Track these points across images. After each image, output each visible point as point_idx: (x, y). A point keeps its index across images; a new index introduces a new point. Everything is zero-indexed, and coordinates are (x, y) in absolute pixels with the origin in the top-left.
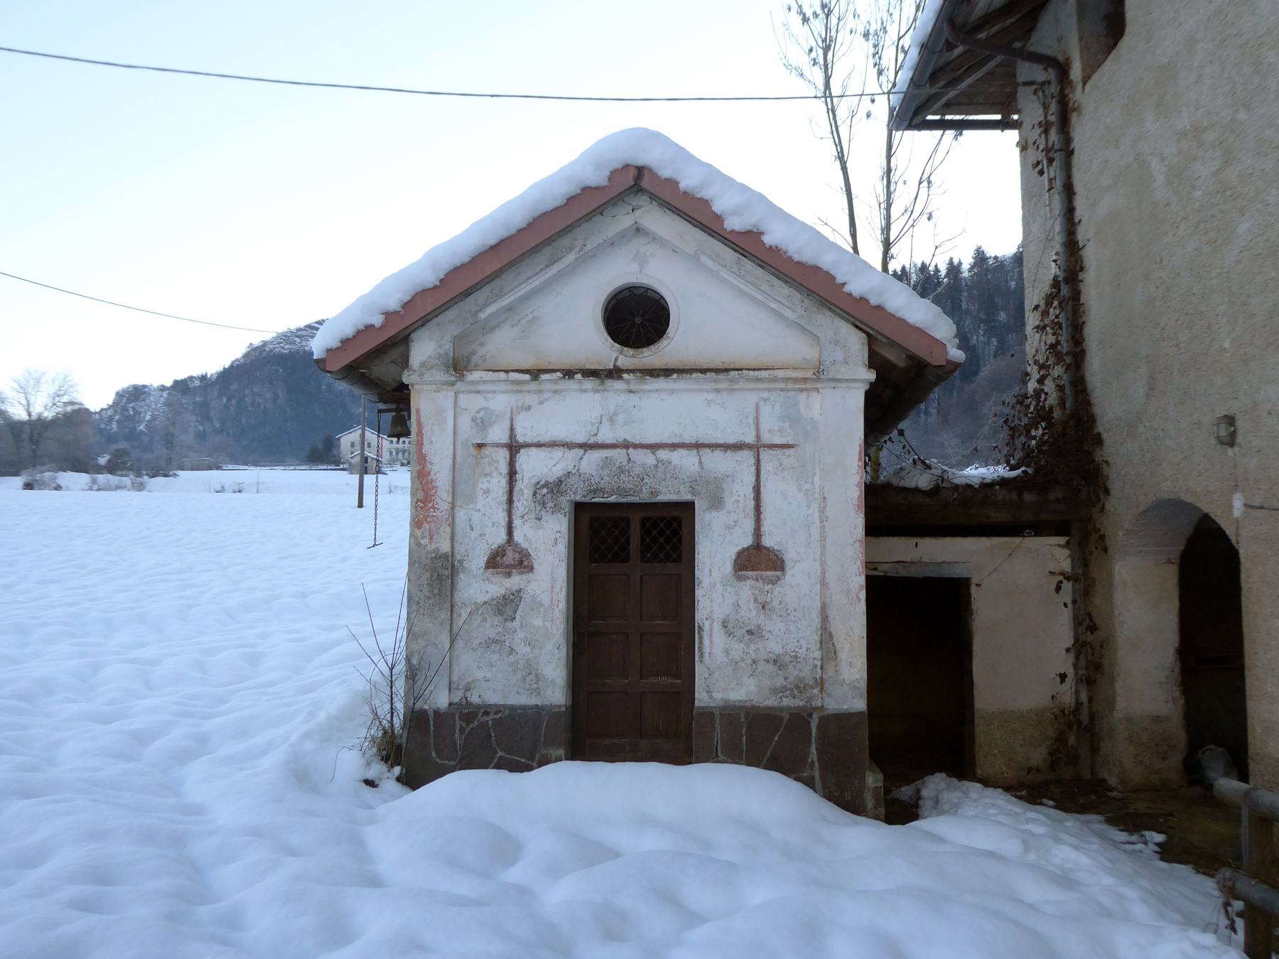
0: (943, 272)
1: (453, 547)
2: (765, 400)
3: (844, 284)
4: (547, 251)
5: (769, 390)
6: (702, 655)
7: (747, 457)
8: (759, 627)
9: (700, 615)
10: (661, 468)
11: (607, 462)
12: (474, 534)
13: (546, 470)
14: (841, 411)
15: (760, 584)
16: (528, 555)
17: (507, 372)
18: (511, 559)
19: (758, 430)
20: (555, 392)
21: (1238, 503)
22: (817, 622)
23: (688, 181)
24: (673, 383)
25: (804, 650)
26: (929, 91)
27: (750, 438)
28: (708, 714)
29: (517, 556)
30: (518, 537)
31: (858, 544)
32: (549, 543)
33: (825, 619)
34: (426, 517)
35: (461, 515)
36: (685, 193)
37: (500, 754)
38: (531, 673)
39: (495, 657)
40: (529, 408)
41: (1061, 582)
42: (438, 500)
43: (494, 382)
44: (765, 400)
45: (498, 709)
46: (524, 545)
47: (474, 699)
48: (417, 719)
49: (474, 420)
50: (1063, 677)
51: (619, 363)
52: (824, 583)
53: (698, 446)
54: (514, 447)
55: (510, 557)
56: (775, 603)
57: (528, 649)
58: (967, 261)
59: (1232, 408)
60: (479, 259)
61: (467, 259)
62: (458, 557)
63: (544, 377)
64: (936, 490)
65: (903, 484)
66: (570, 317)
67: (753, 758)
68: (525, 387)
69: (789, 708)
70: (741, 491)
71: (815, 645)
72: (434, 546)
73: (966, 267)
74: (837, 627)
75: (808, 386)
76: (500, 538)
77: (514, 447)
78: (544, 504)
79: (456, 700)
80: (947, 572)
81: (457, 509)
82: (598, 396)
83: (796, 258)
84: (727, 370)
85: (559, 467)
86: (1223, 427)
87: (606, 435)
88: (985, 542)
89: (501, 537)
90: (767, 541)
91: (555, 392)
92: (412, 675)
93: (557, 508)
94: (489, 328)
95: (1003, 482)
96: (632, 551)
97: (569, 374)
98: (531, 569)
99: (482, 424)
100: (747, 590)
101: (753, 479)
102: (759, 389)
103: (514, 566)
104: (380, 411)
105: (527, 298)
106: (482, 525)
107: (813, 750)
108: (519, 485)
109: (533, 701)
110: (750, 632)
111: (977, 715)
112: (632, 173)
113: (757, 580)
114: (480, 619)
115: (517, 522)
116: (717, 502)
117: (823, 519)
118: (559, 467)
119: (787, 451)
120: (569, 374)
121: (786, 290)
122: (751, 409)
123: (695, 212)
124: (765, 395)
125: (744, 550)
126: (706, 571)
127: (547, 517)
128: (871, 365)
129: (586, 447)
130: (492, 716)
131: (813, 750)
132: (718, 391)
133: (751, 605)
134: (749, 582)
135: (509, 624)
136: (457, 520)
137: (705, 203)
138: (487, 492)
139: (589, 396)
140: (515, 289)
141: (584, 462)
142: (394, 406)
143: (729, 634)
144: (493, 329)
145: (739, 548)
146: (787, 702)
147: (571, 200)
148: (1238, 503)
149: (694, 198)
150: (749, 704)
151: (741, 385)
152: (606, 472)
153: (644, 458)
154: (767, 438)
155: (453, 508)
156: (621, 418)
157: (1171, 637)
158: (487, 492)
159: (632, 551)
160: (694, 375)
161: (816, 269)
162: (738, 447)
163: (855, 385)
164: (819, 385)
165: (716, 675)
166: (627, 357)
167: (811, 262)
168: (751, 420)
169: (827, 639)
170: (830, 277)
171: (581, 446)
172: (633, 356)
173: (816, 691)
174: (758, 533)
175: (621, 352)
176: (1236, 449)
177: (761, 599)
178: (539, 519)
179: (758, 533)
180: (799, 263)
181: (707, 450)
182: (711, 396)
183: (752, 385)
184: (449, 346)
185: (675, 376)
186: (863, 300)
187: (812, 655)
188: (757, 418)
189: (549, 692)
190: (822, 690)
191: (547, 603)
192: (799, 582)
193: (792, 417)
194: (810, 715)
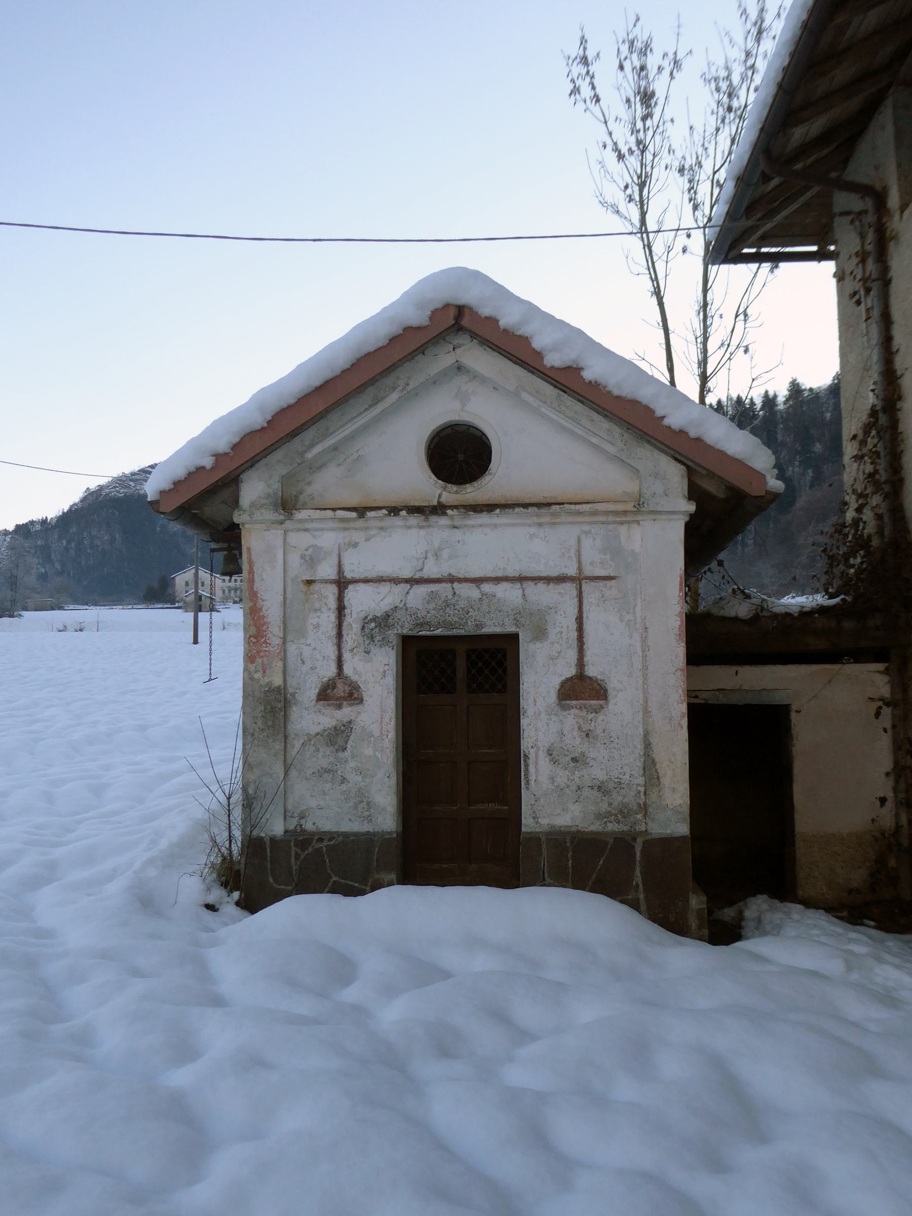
1: (285, 681)
3: (663, 417)
5: (591, 523)
6: (528, 782)
7: (569, 589)
8: (583, 754)
9: (526, 744)
10: (486, 601)
11: (433, 596)
12: (305, 668)
14: (662, 543)
17: (334, 510)
18: (339, 691)
19: (579, 562)
20: (381, 528)
22: (640, 748)
23: (508, 319)
25: (627, 776)
26: (744, 223)
27: (572, 571)
28: (534, 839)
29: (347, 689)
30: (348, 670)
31: (679, 673)
33: (647, 745)
34: (258, 652)
35: (292, 649)
37: (334, 879)
38: (362, 800)
39: (328, 786)
40: (355, 545)
42: (270, 635)
44: (587, 533)
45: (332, 835)
46: (354, 678)
47: (309, 826)
48: (254, 846)
49: (303, 557)
50: (883, 801)
51: (443, 500)
52: (646, 711)
53: (521, 579)
54: (342, 583)
55: (341, 689)
57: (360, 778)
58: (782, 393)
61: (293, 401)
62: (291, 690)
63: (370, 514)
64: (756, 619)
65: (722, 613)
66: (394, 455)
68: (353, 525)
69: (613, 832)
70: (565, 621)
71: (638, 771)
72: (267, 680)
73: (781, 399)
74: (659, 754)
75: (629, 518)
76: (330, 671)
77: (342, 583)
78: (372, 638)
79: (292, 827)
80: (767, 699)
82: (422, 532)
83: (616, 392)
84: (549, 505)
87: (432, 570)
89: (332, 671)
91: (381, 528)
92: (248, 804)
93: (385, 642)
94: (317, 466)
95: (822, 610)
96: (458, 683)
97: (394, 511)
98: (361, 701)
99: (311, 561)
100: (571, 719)
101: (576, 611)
102: (580, 523)
103: (344, 699)
104: (213, 550)
105: (352, 437)
107: (638, 873)
108: (348, 620)
109: (366, 828)
110: (574, 760)
112: (452, 313)
113: (581, 708)
114: (313, 748)
115: (346, 656)
116: (540, 634)
117: (645, 648)
120: (394, 511)
122: (573, 542)
124: (586, 528)
125: (568, 680)
126: (531, 701)
127: (375, 650)
131: (638, 873)
132: (540, 525)
133: (576, 734)
134: (573, 711)
137: (525, 341)
138: (317, 626)
139: (414, 532)
140: (342, 428)
142: (225, 545)
143: (555, 762)
145: (563, 678)
146: (611, 827)
147: (394, 340)
151: (563, 519)
152: (432, 605)
154: (588, 571)
155: (284, 643)
156: (445, 553)
159: (458, 683)
160: (517, 510)
161: (635, 403)
162: (561, 579)
166: (450, 494)
168: (573, 553)
169: (649, 766)
170: (648, 411)
171: (407, 581)
172: (456, 492)
174: (581, 663)
175: (445, 489)
178: (368, 653)
179: (581, 663)
180: (618, 398)
181: (530, 583)
182: (533, 530)
183: (571, 519)
184: (277, 486)
185: (498, 511)
186: (682, 433)
187: (635, 782)
188: (579, 552)
190: (645, 815)
191: (376, 733)
192: (622, 709)
194: (634, 839)
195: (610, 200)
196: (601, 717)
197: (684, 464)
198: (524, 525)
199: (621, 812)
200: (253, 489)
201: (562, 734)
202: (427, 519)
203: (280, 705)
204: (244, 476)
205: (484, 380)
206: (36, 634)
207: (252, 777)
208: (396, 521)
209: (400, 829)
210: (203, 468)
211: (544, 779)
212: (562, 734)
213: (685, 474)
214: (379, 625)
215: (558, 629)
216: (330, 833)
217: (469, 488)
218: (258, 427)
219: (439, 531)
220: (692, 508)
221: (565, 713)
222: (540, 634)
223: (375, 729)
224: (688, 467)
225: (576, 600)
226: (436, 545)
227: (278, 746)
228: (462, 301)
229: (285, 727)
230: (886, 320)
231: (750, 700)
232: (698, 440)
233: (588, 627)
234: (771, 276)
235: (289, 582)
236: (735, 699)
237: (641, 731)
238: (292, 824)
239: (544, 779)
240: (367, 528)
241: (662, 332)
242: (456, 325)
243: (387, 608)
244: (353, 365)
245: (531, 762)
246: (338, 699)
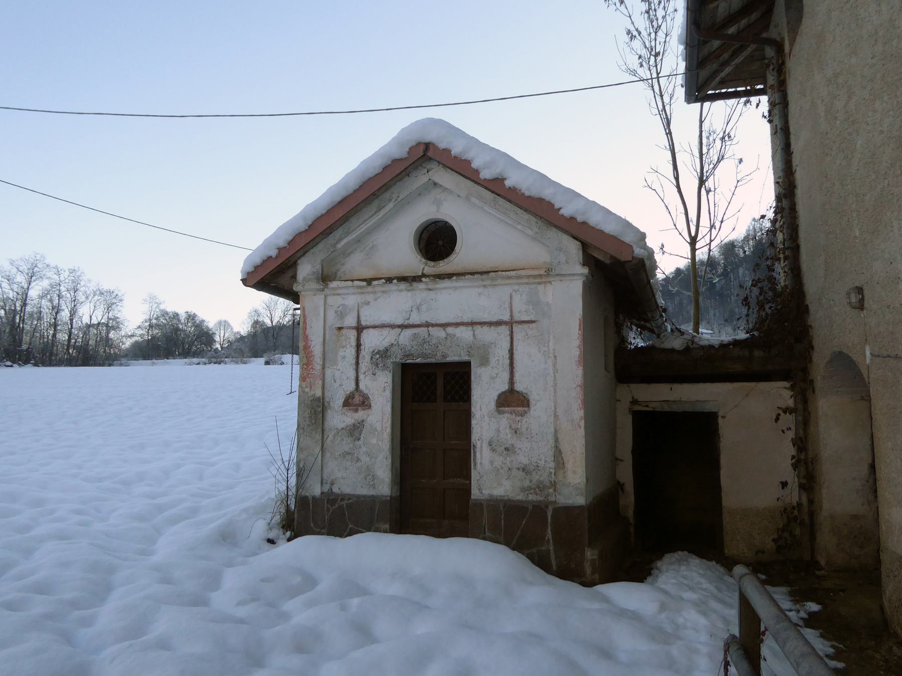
1: (323, 393)
2: (516, 291)
3: (559, 209)
4: (376, 203)
5: (518, 284)
6: (475, 464)
7: (505, 330)
8: (513, 445)
9: (475, 437)
11: (415, 336)
12: (337, 385)
15: (513, 416)
16: (368, 398)
17: (352, 281)
18: (357, 401)
19: (511, 311)
20: (383, 292)
22: (552, 443)
23: (457, 149)
25: (543, 462)
26: (704, 73)
27: (506, 318)
28: (479, 504)
29: (361, 399)
30: (362, 386)
31: (578, 389)
32: (381, 389)
33: (556, 440)
35: (328, 372)
36: (455, 157)
37: (350, 526)
38: (369, 475)
39: (349, 463)
40: (368, 303)
41: (779, 415)
42: (315, 363)
44: (516, 291)
45: (350, 497)
46: (366, 391)
47: (335, 490)
48: (303, 501)
49: (336, 312)
50: (784, 485)
52: (556, 416)
53: (472, 324)
54: (360, 329)
55: (357, 399)
56: (524, 429)
57: (368, 459)
60: (330, 211)
61: (324, 212)
62: (327, 400)
63: (374, 283)
64: (687, 350)
65: (662, 346)
66: (394, 243)
69: (533, 501)
70: (501, 353)
71: (550, 458)
72: (312, 393)
74: (565, 447)
75: (544, 280)
76: (351, 387)
78: (377, 365)
79: (326, 490)
80: (699, 408)
81: (326, 369)
82: (410, 294)
83: (527, 194)
84: (488, 272)
85: (386, 340)
86: (853, 296)
87: (415, 319)
88: (728, 386)
90: (518, 387)
91: (383, 292)
92: (300, 474)
93: (385, 367)
94: (346, 253)
95: (736, 343)
96: (433, 392)
97: (389, 280)
98: (370, 407)
99: (341, 315)
100: (504, 420)
101: (509, 345)
103: (359, 405)
105: (369, 232)
106: (341, 379)
107: (549, 531)
108: (363, 353)
109: (371, 492)
110: (507, 449)
111: (724, 510)
112: (422, 148)
113: (511, 413)
114: (340, 439)
115: (361, 377)
116: (485, 361)
117: (556, 371)
118: (386, 340)
119: (531, 325)
120: (389, 280)
121: (526, 216)
122: (507, 298)
123: (462, 168)
124: (516, 287)
125: (503, 393)
126: (478, 408)
127: (379, 373)
128: (584, 264)
129: (403, 327)
130: (346, 502)
131: (549, 531)
132: (485, 286)
133: (508, 431)
134: (506, 415)
135: (357, 442)
136: (326, 376)
137: (468, 162)
138: (344, 357)
139: (404, 293)
140: (359, 227)
143: (493, 450)
144: (349, 254)
145: (500, 392)
146: (531, 497)
147: (386, 168)
149: (461, 160)
150: (506, 498)
151: (499, 281)
152: (415, 343)
154: (517, 317)
155: (323, 368)
156: (424, 308)
158: (344, 357)
159: (433, 392)
160: (467, 277)
161: (541, 200)
162: (499, 323)
163: (575, 278)
164: (551, 279)
165: (485, 478)
166: (431, 268)
167: (537, 196)
168: (507, 305)
169: (558, 454)
170: (550, 205)
171: (399, 326)
172: (434, 266)
173: (551, 490)
175: (426, 264)
176: (865, 311)
178: (374, 375)
180: (529, 197)
181: (479, 326)
182: (481, 290)
183: (507, 282)
184: (319, 267)
185: (455, 278)
186: (572, 219)
187: (548, 465)
188: (511, 304)
189: (380, 487)
190: (555, 490)
191: (379, 429)
192: (540, 414)
194: (547, 507)
195: (631, 67)
197: (579, 241)
198: (475, 287)
199: (538, 487)
200: (306, 269)
201: (498, 431)
202: (411, 285)
203: (320, 409)
204: (299, 261)
205: (450, 192)
207: (302, 456)
209: (397, 493)
212: (498, 431)
213: (580, 247)
215: (497, 358)
216: (349, 495)
217: (441, 263)
219: (420, 292)
220: (585, 271)
221: (501, 416)
225: (508, 338)
226: (418, 301)
227: (318, 437)
228: (427, 141)
229: (323, 423)
231: (688, 408)
232: (584, 223)
233: (517, 356)
234: (745, 109)
235: (327, 328)
236: (675, 408)
237: (552, 430)
238: (326, 488)
240: (375, 292)
241: (669, 153)
242: (425, 157)
243: (387, 345)
244: (360, 187)
245: (478, 450)
246: (356, 405)
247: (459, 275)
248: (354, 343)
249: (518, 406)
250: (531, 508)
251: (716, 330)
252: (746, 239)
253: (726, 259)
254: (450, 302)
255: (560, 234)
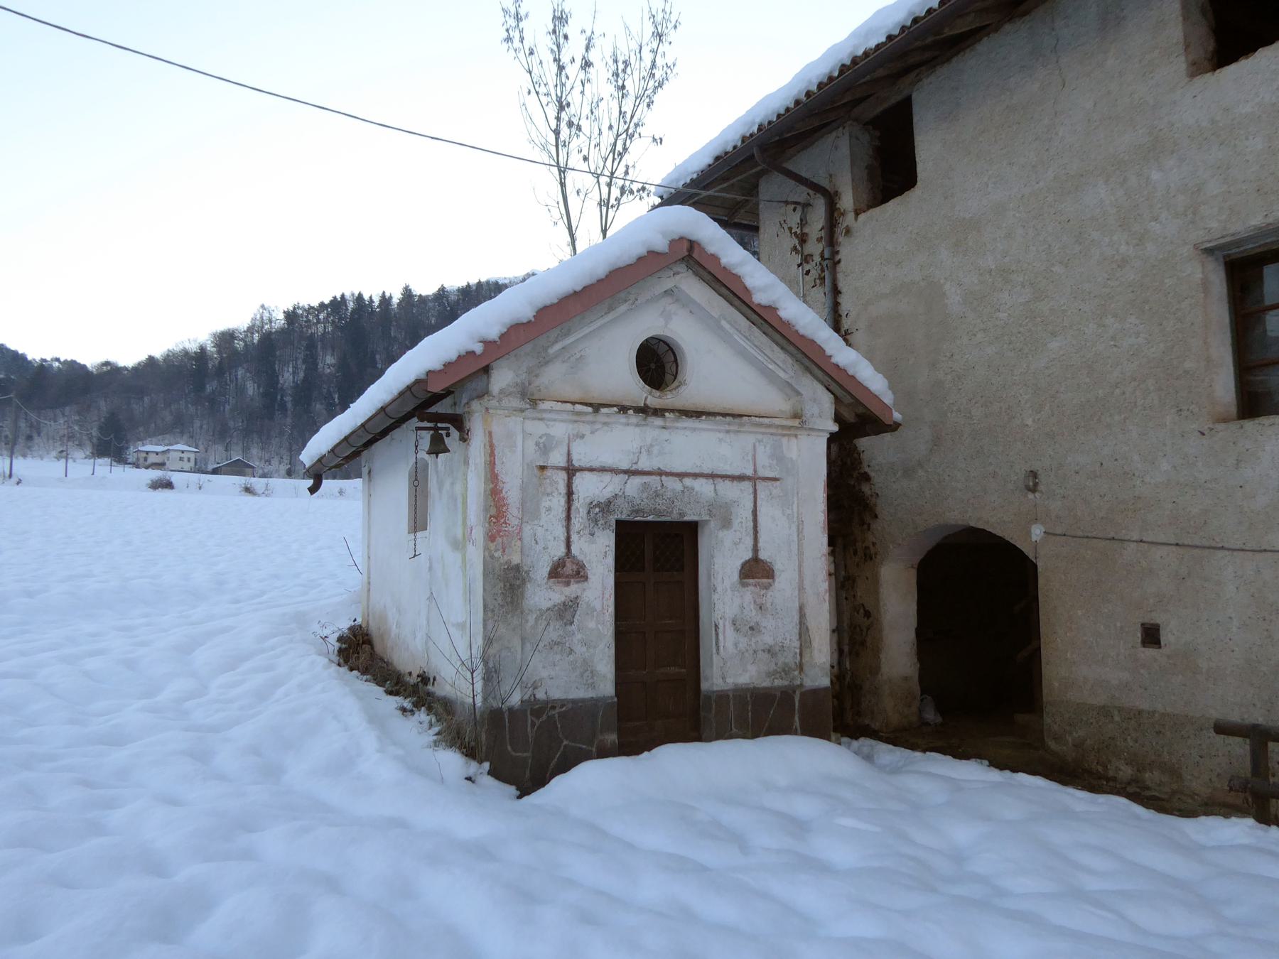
0: (376, 303)
5: (763, 433)
7: (747, 485)
10: (687, 493)
11: (645, 486)
12: (538, 548)
13: (597, 492)
17: (573, 403)
18: (567, 570)
21: (1037, 532)
22: (796, 619)
24: (702, 424)
27: (749, 472)
29: (575, 567)
32: (599, 553)
34: (499, 532)
35: (527, 530)
37: (565, 742)
38: (587, 669)
39: (558, 657)
40: (582, 437)
42: (509, 516)
43: (558, 412)
45: (563, 703)
46: (580, 557)
47: (541, 695)
49: (537, 444)
51: (648, 402)
52: (801, 588)
53: (712, 476)
54: (571, 471)
55: (570, 567)
56: (768, 605)
57: (584, 649)
58: (397, 297)
59: (1036, 466)
63: (604, 410)
66: (610, 362)
67: (813, 729)
69: (780, 687)
70: (743, 515)
72: (506, 558)
73: (395, 301)
74: (811, 623)
77: (571, 471)
78: (596, 521)
79: (526, 697)
82: (637, 430)
83: (802, 331)
84: (741, 416)
85: (610, 489)
87: (644, 464)
89: (561, 551)
93: (606, 526)
96: (657, 556)
98: (586, 578)
99: (545, 448)
100: (749, 594)
102: (756, 433)
103: (572, 576)
106: (543, 540)
107: (797, 719)
108: (576, 504)
110: (752, 628)
112: (686, 245)
114: (544, 623)
115: (574, 537)
116: (726, 523)
120: (623, 409)
124: (760, 437)
126: (720, 579)
127: (598, 533)
130: (558, 710)
131: (797, 719)
132: (728, 432)
135: (569, 628)
138: (549, 509)
139: (631, 429)
141: (628, 486)
143: (737, 630)
146: (778, 683)
148: (1037, 532)
152: (645, 495)
153: (673, 485)
154: (761, 473)
156: (655, 450)
157: (913, 622)
158: (549, 509)
159: (657, 556)
160: (718, 418)
161: (813, 342)
162: (741, 478)
166: (654, 399)
168: (750, 458)
171: (625, 472)
173: (796, 673)
174: (756, 549)
176: (1037, 495)
177: (759, 601)
178: (592, 535)
179: (756, 549)
180: (803, 336)
182: (721, 435)
193: (778, 457)
196: (770, 593)
202: (645, 419)
206: (66, 499)
208: (622, 418)
210: (473, 353)
211: (730, 645)
214: (602, 511)
218: (525, 321)
219: (652, 431)
222: (726, 523)
223: (597, 605)
224: (836, 398)
226: (649, 441)
228: (693, 238)
230: (836, 292)
232: (853, 377)
233: (760, 519)
239: (730, 645)
240: (593, 423)
246: (567, 577)
247: (696, 414)
248: (563, 489)
249: (763, 577)
250: (778, 694)
251: (201, 447)
252: (251, 330)
253: (219, 352)
254: (688, 446)
255: (815, 382)
